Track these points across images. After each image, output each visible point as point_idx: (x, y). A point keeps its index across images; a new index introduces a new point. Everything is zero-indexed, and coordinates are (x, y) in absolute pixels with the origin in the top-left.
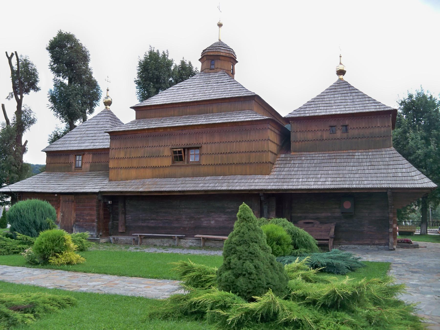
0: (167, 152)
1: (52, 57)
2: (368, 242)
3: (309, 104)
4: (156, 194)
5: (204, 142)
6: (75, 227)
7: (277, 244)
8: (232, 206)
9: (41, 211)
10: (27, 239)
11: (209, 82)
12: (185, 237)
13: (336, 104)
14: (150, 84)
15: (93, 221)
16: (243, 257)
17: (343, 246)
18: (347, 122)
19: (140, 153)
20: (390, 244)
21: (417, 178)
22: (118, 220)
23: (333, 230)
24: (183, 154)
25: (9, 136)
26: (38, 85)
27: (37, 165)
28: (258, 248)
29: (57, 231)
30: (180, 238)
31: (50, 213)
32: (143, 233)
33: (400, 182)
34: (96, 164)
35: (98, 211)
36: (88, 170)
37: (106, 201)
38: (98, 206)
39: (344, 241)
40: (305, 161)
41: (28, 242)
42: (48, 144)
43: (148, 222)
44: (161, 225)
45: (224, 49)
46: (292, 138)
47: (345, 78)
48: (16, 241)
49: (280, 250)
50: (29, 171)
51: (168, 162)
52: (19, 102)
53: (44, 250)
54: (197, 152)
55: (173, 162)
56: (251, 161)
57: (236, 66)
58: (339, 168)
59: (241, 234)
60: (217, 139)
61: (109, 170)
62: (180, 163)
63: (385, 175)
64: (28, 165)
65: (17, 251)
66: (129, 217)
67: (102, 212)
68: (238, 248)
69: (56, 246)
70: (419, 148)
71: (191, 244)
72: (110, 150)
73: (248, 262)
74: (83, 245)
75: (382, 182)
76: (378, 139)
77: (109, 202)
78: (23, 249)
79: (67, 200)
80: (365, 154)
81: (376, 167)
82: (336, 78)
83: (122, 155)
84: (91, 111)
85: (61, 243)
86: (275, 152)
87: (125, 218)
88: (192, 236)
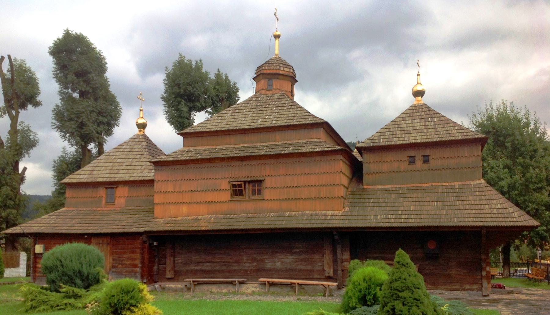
0: (225, 185)
1: (57, 64)
2: (457, 287)
3: (382, 133)
5: (268, 174)
8: (300, 245)
10: (73, 292)
14: (180, 101)
15: (136, 266)
16: (408, 303)
18: (428, 152)
22: (165, 264)
24: (243, 188)
25: (6, 162)
26: (39, 98)
30: (241, 283)
32: (196, 278)
35: (142, 254)
37: (151, 242)
43: (203, 265)
44: (218, 268)
46: (365, 170)
48: (61, 294)
51: (227, 196)
52: (14, 120)
53: (115, 304)
55: (232, 196)
56: (322, 196)
62: (239, 198)
64: (29, 197)
65: (62, 307)
67: (146, 256)
70: (503, 179)
71: (253, 289)
76: (465, 170)
77: (155, 244)
83: (170, 189)
86: (346, 185)
87: (174, 261)
88: (257, 279)
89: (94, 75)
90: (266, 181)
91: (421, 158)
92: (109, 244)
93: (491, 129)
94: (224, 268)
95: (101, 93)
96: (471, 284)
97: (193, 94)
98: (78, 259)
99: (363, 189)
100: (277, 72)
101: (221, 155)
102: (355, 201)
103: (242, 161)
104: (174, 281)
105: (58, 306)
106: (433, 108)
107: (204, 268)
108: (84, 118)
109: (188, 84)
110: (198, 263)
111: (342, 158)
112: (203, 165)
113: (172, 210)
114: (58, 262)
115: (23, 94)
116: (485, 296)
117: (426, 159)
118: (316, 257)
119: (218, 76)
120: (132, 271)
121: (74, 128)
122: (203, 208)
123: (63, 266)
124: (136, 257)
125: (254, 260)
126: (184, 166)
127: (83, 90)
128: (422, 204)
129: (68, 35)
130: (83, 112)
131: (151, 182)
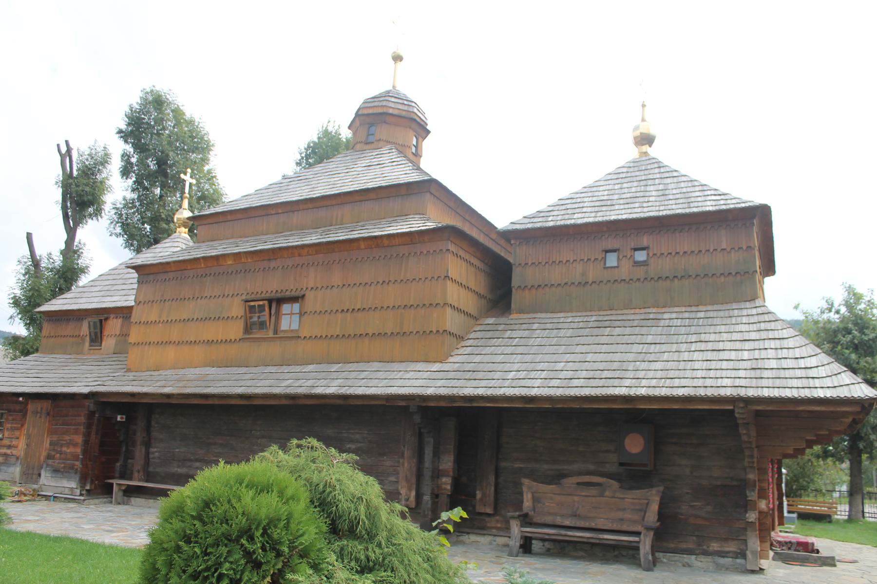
0: (237, 309)
3: (562, 203)
5: (311, 284)
8: (358, 436)
13: (622, 202)
20: (749, 555)
23: (655, 507)
33: (770, 383)
35: (87, 435)
36: (112, 351)
37: (108, 413)
38: (89, 426)
40: (538, 331)
43: (190, 466)
45: (396, 100)
46: (515, 282)
47: (652, 151)
51: (236, 330)
54: (296, 307)
55: (248, 329)
58: (613, 348)
60: (337, 278)
63: (731, 365)
75: (719, 382)
76: (722, 279)
79: (39, 410)
80: (687, 315)
81: (710, 346)
82: (632, 153)
83: (153, 317)
86: (472, 310)
96: (726, 540)
111: (452, 247)
118: (388, 462)
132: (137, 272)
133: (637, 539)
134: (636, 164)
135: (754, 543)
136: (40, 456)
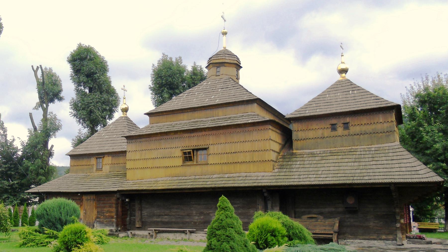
0: (179, 153)
2: (375, 237)
4: (168, 192)
6: (96, 223)
7: (272, 235)
8: (238, 202)
9: (67, 209)
10: (53, 234)
11: (214, 88)
12: (195, 231)
15: (112, 217)
17: (348, 240)
18: (348, 120)
19: (154, 154)
20: (398, 239)
21: (422, 172)
22: (135, 216)
23: (337, 225)
26: (62, 95)
27: (62, 167)
28: (234, 233)
29: (78, 225)
30: (191, 232)
31: (75, 211)
34: (116, 165)
35: (117, 208)
37: (123, 198)
38: (117, 204)
39: (350, 236)
41: (54, 236)
42: (72, 148)
44: (174, 220)
46: (294, 137)
47: (348, 76)
48: (44, 235)
49: (274, 241)
50: (55, 173)
51: (179, 161)
52: (45, 111)
53: (67, 242)
57: (241, 71)
59: (219, 221)
61: (126, 171)
64: (55, 167)
65: (44, 244)
66: (145, 213)
67: (120, 209)
68: (217, 232)
69: (78, 238)
70: (437, 142)
72: (127, 152)
73: (225, 244)
74: (102, 240)
76: (381, 134)
78: (50, 242)
83: (137, 157)
84: (111, 117)
85: (82, 235)
87: (141, 214)
89: (98, 75)
90: (210, 148)
91: (341, 125)
92: (94, 200)
93: (426, 99)
94: (179, 220)
95: (104, 88)
96: (388, 234)
97: (173, 84)
98: (59, 210)
99: (293, 153)
100: (224, 61)
101: (175, 129)
102: (285, 163)
103: (191, 133)
104: (141, 230)
105: (42, 243)
106: (354, 82)
107: (164, 220)
108: (92, 107)
109: (169, 76)
110: (159, 216)
111: (271, 127)
112: (162, 137)
113: (139, 174)
114: (45, 212)
115: (51, 91)
116: (400, 245)
117: (346, 126)
119: (194, 68)
120: (110, 221)
121: (85, 115)
122: (162, 172)
123: (48, 215)
124: (112, 210)
125: (201, 213)
126: (148, 139)
127: (91, 86)
128: (340, 164)
129: (80, 46)
130: (91, 103)
131: (124, 153)
132: (127, 139)
133: (331, 236)
134: (340, 83)
135: (399, 235)
136: (92, 218)
